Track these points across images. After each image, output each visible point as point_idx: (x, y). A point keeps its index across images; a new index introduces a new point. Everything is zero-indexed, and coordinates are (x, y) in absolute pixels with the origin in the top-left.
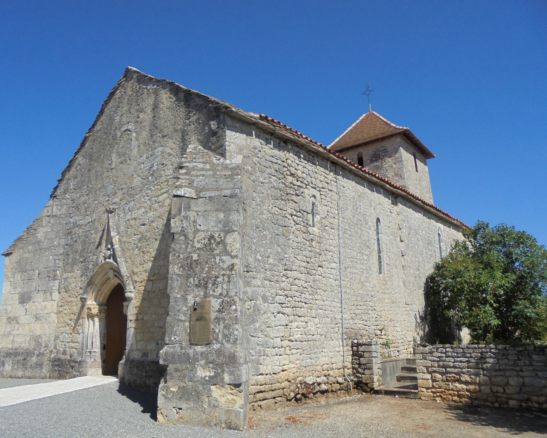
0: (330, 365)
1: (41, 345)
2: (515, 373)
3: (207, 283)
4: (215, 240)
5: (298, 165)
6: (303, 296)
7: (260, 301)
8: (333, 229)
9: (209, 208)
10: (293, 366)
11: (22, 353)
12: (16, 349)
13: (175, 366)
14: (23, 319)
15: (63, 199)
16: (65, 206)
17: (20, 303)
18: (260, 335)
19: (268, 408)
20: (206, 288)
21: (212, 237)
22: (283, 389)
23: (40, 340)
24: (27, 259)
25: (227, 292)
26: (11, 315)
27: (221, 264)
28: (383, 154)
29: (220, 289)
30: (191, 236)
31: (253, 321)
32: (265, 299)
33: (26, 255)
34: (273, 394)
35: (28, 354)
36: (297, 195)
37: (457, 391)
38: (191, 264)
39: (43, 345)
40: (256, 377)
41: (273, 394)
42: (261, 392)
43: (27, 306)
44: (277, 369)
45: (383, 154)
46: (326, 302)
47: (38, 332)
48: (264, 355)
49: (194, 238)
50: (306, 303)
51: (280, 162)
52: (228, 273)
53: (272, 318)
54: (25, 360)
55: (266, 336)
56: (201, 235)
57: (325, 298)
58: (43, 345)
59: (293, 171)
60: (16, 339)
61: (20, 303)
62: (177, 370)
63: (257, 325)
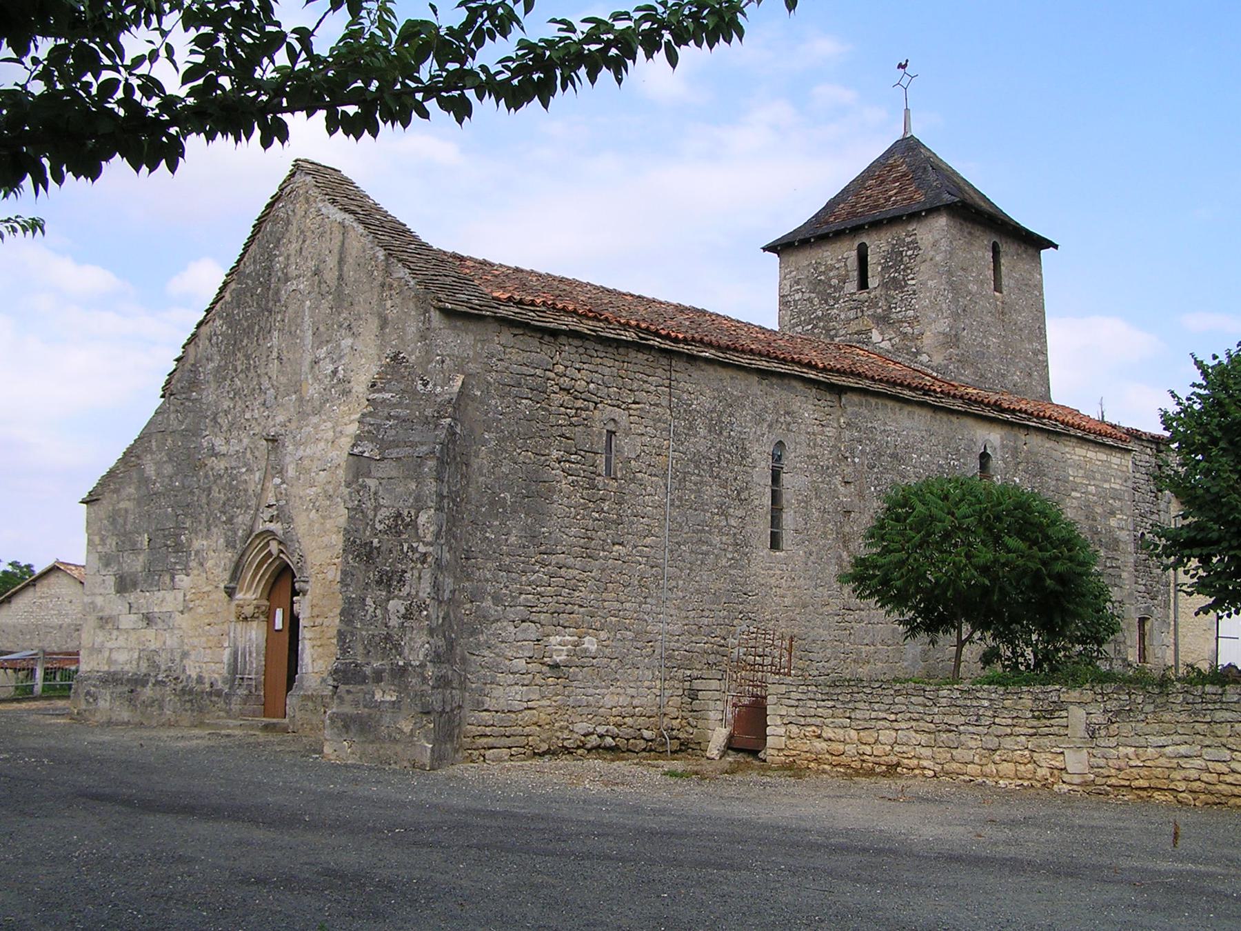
0: (630, 709)
1: (158, 667)
2: (888, 724)
3: (390, 579)
4: (403, 520)
5: (579, 370)
6: (577, 594)
7: (488, 603)
8: (655, 475)
9: (394, 473)
10: (548, 703)
11: (128, 680)
12: (115, 673)
13: (347, 687)
14: (128, 621)
15: (187, 399)
16: (191, 415)
17: (118, 592)
18: (486, 653)
19: (500, 760)
20: (390, 585)
21: (399, 515)
22: (528, 736)
23: (156, 658)
24: (126, 511)
25: (417, 592)
26: (105, 614)
27: (410, 554)
28: (910, 253)
29: (407, 588)
30: (371, 514)
31: (473, 633)
32: (497, 600)
33: (122, 505)
34: (508, 742)
35: (138, 681)
36: (571, 424)
37: (817, 754)
38: (371, 552)
39: (163, 667)
40: (477, 713)
41: (508, 742)
42: (486, 736)
43: (132, 597)
44: (517, 705)
45: (910, 253)
46: (628, 605)
47: (153, 646)
48: (492, 683)
49: (375, 516)
50: (581, 606)
51: (538, 372)
52: (419, 565)
53: (511, 629)
54: (132, 691)
55: (498, 655)
56: (383, 513)
57: (623, 598)
58: (163, 667)
59: (565, 382)
60: (115, 656)
61: (118, 592)
62: (348, 692)
63: (482, 638)
